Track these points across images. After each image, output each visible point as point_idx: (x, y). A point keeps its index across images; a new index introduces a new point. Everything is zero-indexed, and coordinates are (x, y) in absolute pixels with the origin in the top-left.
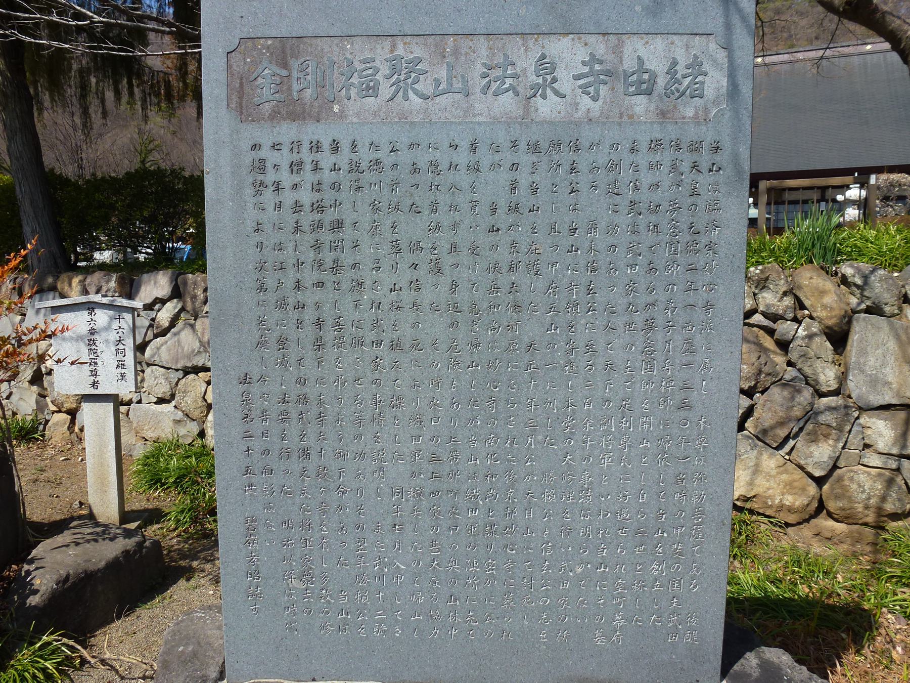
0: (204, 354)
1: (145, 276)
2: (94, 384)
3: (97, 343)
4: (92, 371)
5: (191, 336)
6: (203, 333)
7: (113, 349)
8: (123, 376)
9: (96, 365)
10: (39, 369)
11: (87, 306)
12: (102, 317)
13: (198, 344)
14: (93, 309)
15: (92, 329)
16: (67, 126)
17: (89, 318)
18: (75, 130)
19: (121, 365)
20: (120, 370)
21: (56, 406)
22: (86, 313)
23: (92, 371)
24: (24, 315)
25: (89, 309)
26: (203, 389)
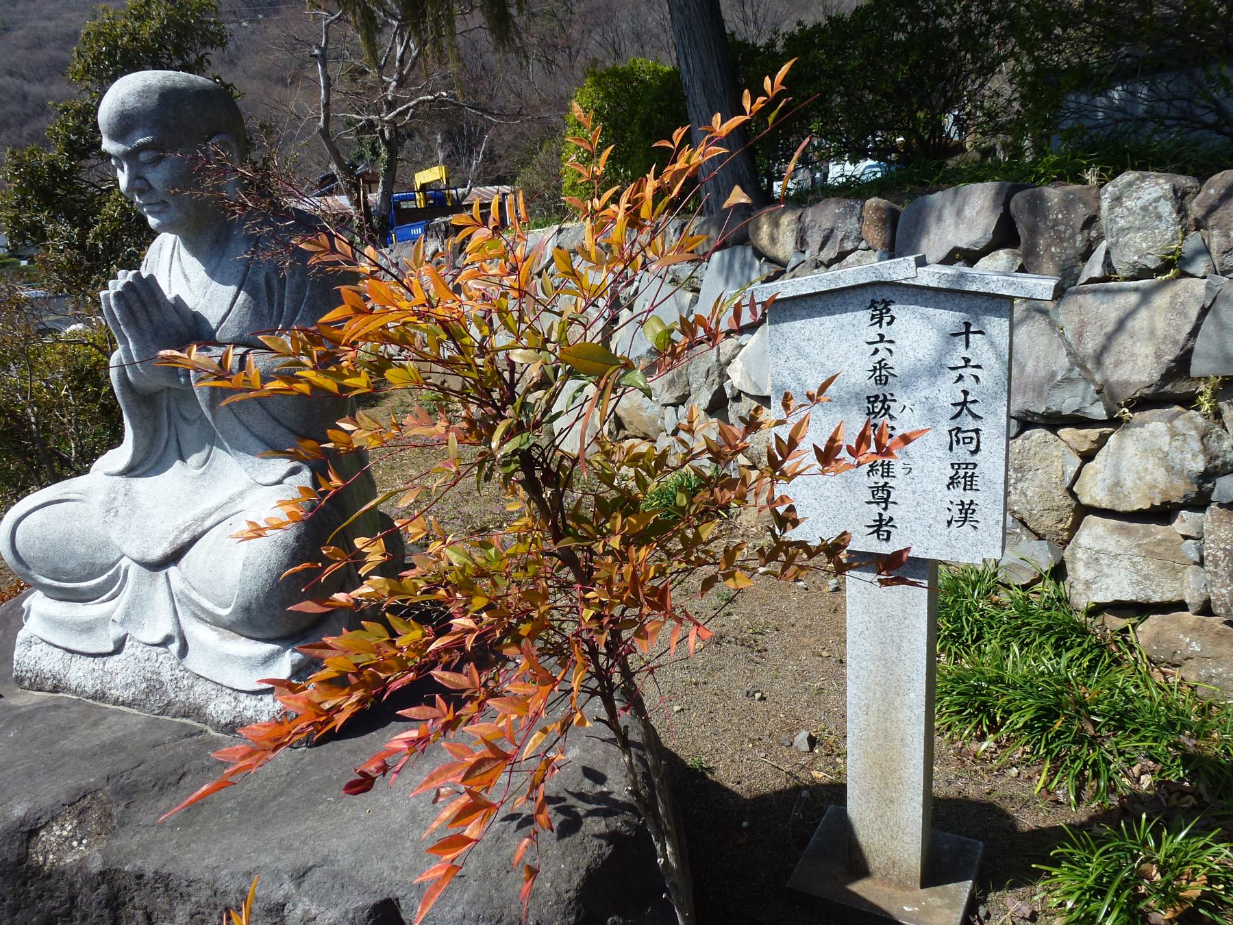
0: (1081, 386)
1: (937, 197)
2: (881, 527)
3: (895, 408)
4: (875, 489)
5: (1043, 341)
6: (1080, 335)
7: (945, 426)
8: (966, 512)
9: (887, 472)
10: (721, 390)
11: (869, 297)
12: (916, 333)
13: (1064, 361)
14: (887, 304)
15: (882, 365)
16: (737, 21)
17: (873, 333)
18: (746, 24)
19: (963, 477)
20: (958, 494)
21: (750, 459)
22: (864, 316)
23: (875, 489)
24: (697, 291)
25: (873, 305)
26: (1071, 470)
